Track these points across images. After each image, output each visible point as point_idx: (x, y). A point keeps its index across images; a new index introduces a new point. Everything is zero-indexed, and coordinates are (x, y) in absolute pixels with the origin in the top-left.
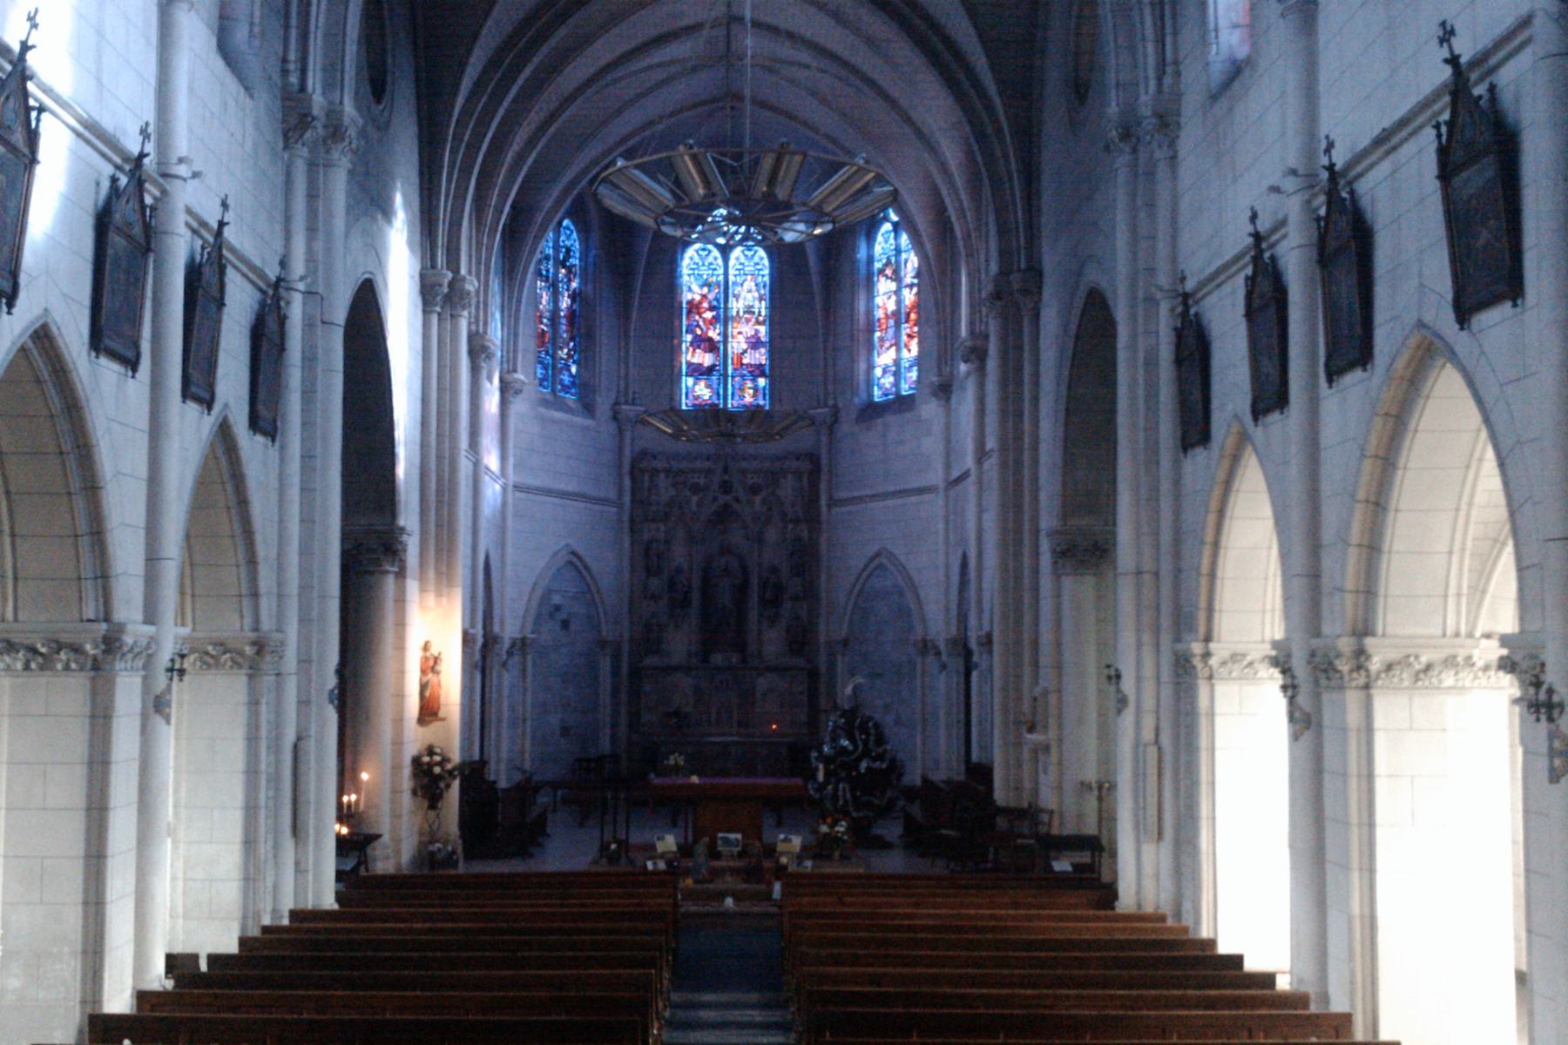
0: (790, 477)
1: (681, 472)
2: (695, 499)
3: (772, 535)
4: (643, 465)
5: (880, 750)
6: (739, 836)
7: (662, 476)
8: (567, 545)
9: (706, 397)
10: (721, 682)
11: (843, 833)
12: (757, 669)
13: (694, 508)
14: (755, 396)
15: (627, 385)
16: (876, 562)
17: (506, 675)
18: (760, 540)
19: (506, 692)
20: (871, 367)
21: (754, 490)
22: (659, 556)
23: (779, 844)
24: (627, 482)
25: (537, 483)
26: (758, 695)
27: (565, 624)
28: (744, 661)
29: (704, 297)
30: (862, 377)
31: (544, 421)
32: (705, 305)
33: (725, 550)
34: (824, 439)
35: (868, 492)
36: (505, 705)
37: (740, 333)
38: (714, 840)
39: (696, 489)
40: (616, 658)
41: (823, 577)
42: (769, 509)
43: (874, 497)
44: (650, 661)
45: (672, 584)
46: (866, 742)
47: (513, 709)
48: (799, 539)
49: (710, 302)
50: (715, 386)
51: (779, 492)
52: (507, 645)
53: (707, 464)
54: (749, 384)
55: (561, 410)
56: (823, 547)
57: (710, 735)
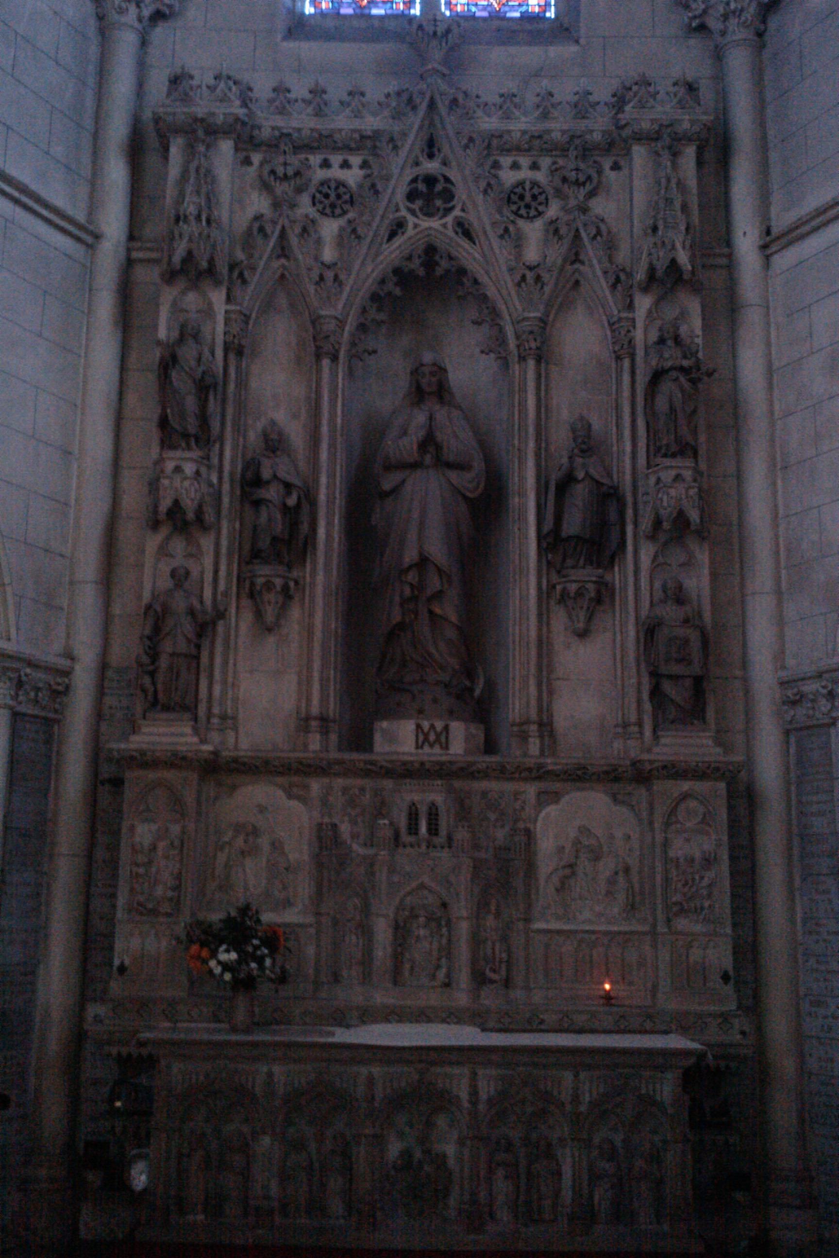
2: (329, 228)
7: (226, 146)
10: (413, 816)
12: (539, 774)
13: (328, 254)
28: (490, 746)
57: (340, 1019)
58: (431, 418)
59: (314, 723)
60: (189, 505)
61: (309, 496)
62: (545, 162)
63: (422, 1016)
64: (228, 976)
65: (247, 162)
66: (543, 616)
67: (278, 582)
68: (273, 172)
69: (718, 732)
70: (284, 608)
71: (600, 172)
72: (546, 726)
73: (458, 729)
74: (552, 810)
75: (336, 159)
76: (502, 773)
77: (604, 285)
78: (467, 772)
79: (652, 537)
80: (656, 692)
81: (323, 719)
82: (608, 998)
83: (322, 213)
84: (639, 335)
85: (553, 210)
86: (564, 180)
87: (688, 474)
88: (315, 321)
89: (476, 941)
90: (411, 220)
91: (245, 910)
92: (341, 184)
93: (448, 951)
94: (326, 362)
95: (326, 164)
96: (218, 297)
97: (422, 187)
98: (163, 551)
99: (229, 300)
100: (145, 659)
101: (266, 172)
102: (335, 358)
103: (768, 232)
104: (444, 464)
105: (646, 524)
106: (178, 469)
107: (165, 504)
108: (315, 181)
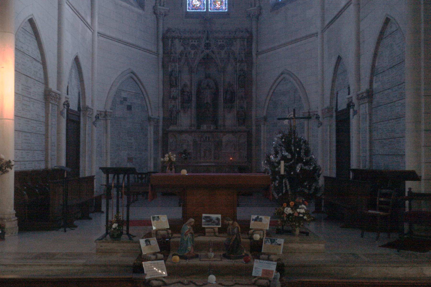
2: (193, 52)
3: (230, 68)
6: (219, 216)
7: (177, 41)
8: (130, 69)
9: (198, 6)
10: (206, 138)
11: (303, 214)
13: (193, 56)
14: (221, 5)
16: (282, 77)
21: (222, 47)
23: (252, 222)
24: (161, 44)
27: (129, 108)
28: (216, 129)
33: (208, 76)
35: (276, 44)
36: (95, 144)
38: (198, 219)
39: (194, 47)
40: (156, 127)
43: (280, 46)
44: (172, 128)
45: (183, 92)
46: (299, 153)
51: (233, 48)
52: (95, 114)
53: (199, 35)
56: (254, 76)
57: (200, 163)
60: (175, 96)
61: (191, 93)
63: (207, 162)
64: (184, 158)
65: (180, 41)
67: (187, 106)
72: (224, 126)
75: (194, 41)
82: (231, 160)
83: (192, 49)
85: (226, 49)
86: (227, 44)
91: (185, 150)
92: (194, 45)
95: (192, 41)
96: (177, 64)
97: (206, 45)
99: (179, 64)
101: (183, 43)
107: (172, 96)
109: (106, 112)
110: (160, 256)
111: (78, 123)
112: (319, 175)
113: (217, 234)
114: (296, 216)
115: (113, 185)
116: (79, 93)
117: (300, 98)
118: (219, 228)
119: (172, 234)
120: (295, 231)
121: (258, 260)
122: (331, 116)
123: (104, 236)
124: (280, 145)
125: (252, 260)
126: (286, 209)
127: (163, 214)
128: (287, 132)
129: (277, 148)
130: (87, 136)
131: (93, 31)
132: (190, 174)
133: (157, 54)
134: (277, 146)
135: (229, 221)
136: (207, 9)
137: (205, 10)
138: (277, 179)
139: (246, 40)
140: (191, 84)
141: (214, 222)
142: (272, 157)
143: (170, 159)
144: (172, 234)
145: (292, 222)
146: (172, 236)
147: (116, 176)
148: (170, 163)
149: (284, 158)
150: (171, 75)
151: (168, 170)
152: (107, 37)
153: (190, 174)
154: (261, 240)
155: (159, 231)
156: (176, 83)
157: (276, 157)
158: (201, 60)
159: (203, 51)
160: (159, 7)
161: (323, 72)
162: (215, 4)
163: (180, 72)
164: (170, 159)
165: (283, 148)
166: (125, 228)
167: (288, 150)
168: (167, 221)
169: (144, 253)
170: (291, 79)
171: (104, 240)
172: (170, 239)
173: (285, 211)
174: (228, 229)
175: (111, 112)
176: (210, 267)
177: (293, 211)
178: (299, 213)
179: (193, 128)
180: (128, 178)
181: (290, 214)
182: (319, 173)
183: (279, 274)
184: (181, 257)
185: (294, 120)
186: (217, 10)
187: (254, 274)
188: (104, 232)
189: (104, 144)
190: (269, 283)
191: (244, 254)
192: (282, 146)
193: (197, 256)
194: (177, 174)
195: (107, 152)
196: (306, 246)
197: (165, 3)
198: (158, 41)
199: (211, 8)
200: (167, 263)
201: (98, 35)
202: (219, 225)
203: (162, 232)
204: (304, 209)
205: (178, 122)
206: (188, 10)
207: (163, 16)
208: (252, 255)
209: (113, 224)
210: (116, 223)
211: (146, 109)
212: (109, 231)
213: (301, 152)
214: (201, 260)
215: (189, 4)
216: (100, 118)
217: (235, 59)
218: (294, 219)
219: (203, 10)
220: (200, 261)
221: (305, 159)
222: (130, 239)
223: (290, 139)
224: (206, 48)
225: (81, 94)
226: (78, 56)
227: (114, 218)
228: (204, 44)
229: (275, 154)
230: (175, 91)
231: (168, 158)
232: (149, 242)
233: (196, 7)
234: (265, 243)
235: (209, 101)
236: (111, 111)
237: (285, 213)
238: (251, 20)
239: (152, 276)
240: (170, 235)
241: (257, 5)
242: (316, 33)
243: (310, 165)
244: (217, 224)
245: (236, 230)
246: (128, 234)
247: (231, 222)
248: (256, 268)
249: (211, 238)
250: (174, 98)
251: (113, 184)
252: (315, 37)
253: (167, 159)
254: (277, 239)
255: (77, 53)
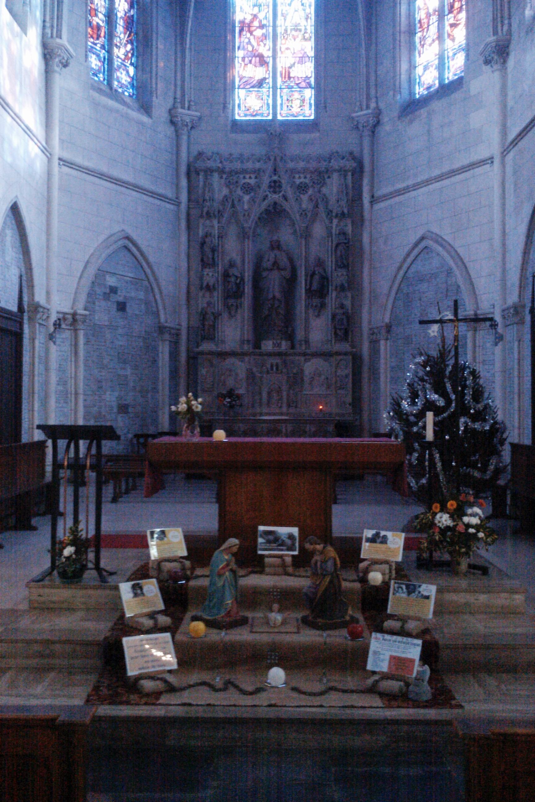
0: (335, 176)
1: (232, 173)
2: (246, 198)
3: (318, 230)
4: (200, 164)
5: (480, 406)
6: (295, 531)
7: (216, 175)
8: (123, 230)
10: (272, 366)
11: (478, 528)
12: (305, 354)
13: (246, 207)
15: (183, 95)
17: (53, 348)
18: (307, 235)
19: (53, 365)
20: (412, 67)
21: (302, 188)
22: (213, 250)
23: (366, 546)
24: (184, 182)
25: (90, 164)
26: (307, 379)
27: (122, 307)
28: (293, 347)
29: (255, 16)
30: (404, 77)
31: (96, 105)
32: (256, 23)
33: (276, 246)
34: (366, 142)
35: (410, 182)
36: (54, 378)
37: (288, 49)
39: (247, 189)
40: (175, 345)
41: (366, 271)
42: (317, 206)
43: (416, 186)
44: (206, 346)
45: (226, 275)
46: (461, 396)
47: (62, 382)
48: (343, 233)
49: (260, 22)
50: (265, 97)
51: (324, 190)
52: (54, 317)
53: (258, 165)
54: (296, 95)
55: (117, 100)
56: (366, 239)
57: (261, 414)
58: (276, 256)
59: (246, 342)
60: (211, 284)
61: (242, 279)
62: (308, 176)
63: (274, 414)
65: (221, 178)
66: (306, 312)
67: (235, 304)
68: (229, 182)
69: (352, 342)
70: (236, 311)
71: (324, 180)
72: (307, 342)
73: (284, 343)
74: (309, 363)
75: (247, 176)
76: (295, 354)
77: (324, 215)
78: (286, 354)
79: (336, 290)
80: (335, 333)
81: (248, 341)
82: (321, 410)
84: (334, 231)
85: (310, 192)
86: (314, 183)
87: (345, 273)
88: (243, 228)
89: (288, 395)
90: (270, 195)
91: (231, 389)
92: (249, 184)
93: (281, 399)
94: (247, 240)
96: (215, 222)
97: (273, 184)
98: (204, 296)
99: (219, 223)
100: (201, 326)
102: (248, 238)
103: (373, 197)
104: (279, 269)
105: (334, 288)
106: (208, 274)
108: (242, 183)
109: (74, 315)
110: (164, 620)
111: (18, 336)
112: (502, 442)
113: (290, 570)
114: (460, 533)
115: (66, 463)
116: (21, 277)
117: (459, 287)
118: (293, 556)
119: (193, 569)
120: (459, 564)
121: (379, 635)
122: (522, 322)
123: (49, 573)
124: (422, 380)
125: (366, 634)
126: (438, 516)
127: (174, 526)
128: (434, 353)
129: (416, 385)
130: (37, 360)
131: (50, 154)
132: (234, 439)
133: (175, 201)
134: (415, 381)
135: (316, 544)
136: (275, 114)
137: (270, 117)
138: (415, 450)
139: (350, 174)
140: (243, 261)
141: (283, 544)
142: (405, 404)
143: (190, 408)
144: (193, 569)
145: (452, 543)
146: (192, 573)
147: (72, 445)
148: (188, 416)
149: (429, 406)
150: (203, 244)
151: (185, 431)
152: (77, 168)
153: (234, 439)
154: (386, 585)
155: (163, 563)
156: (213, 259)
157: (413, 403)
158: (261, 214)
159: (267, 196)
160: (180, 110)
161: (504, 233)
162: (290, 104)
163: (220, 237)
164: (190, 408)
165: (428, 386)
166: (91, 556)
167: (439, 389)
168: (183, 541)
169: (129, 614)
170: (440, 249)
171: (46, 582)
172: (188, 579)
173: (436, 522)
174: (313, 561)
175: (86, 316)
176: (274, 647)
177: (454, 520)
178: (468, 526)
179: (246, 348)
180: (99, 447)
181: (448, 528)
182: (502, 436)
183: (427, 667)
184: (210, 624)
185: (456, 324)
186: (293, 115)
187: (369, 667)
188: (47, 564)
189: (71, 378)
190: (404, 689)
191: (348, 618)
192: (426, 381)
193: (244, 622)
194: (205, 440)
195: (76, 394)
196: (483, 598)
197: (192, 103)
198: (178, 176)
199: (282, 112)
200: (178, 637)
201: (59, 164)
202: (295, 550)
203: (167, 566)
204: (477, 517)
205: (216, 335)
206: (237, 117)
207: (189, 128)
208: (366, 619)
209: (64, 548)
210: (72, 545)
211: (155, 309)
212: (57, 562)
213: (464, 394)
214: (254, 630)
215: (239, 106)
216: (63, 326)
217: (329, 213)
218: (456, 539)
219: (266, 117)
220: (252, 632)
221: (474, 409)
222: (103, 579)
223: (442, 366)
224: (272, 190)
225: (24, 278)
226: (18, 202)
227: (68, 534)
228: (268, 181)
229: (410, 397)
230: (211, 274)
231: (185, 406)
232: (141, 588)
233: (253, 112)
234: (394, 594)
235: (278, 295)
236: (87, 313)
237: (438, 525)
238: (361, 137)
239: (143, 668)
240: (188, 573)
241: (373, 105)
242: (490, 159)
243: (485, 420)
244: (291, 548)
245: (330, 564)
246: (97, 567)
247: (319, 547)
248: (375, 653)
249: (276, 578)
250: (209, 288)
251: (66, 460)
252: (488, 166)
253: (183, 407)
254: (420, 586)
255: (17, 197)
